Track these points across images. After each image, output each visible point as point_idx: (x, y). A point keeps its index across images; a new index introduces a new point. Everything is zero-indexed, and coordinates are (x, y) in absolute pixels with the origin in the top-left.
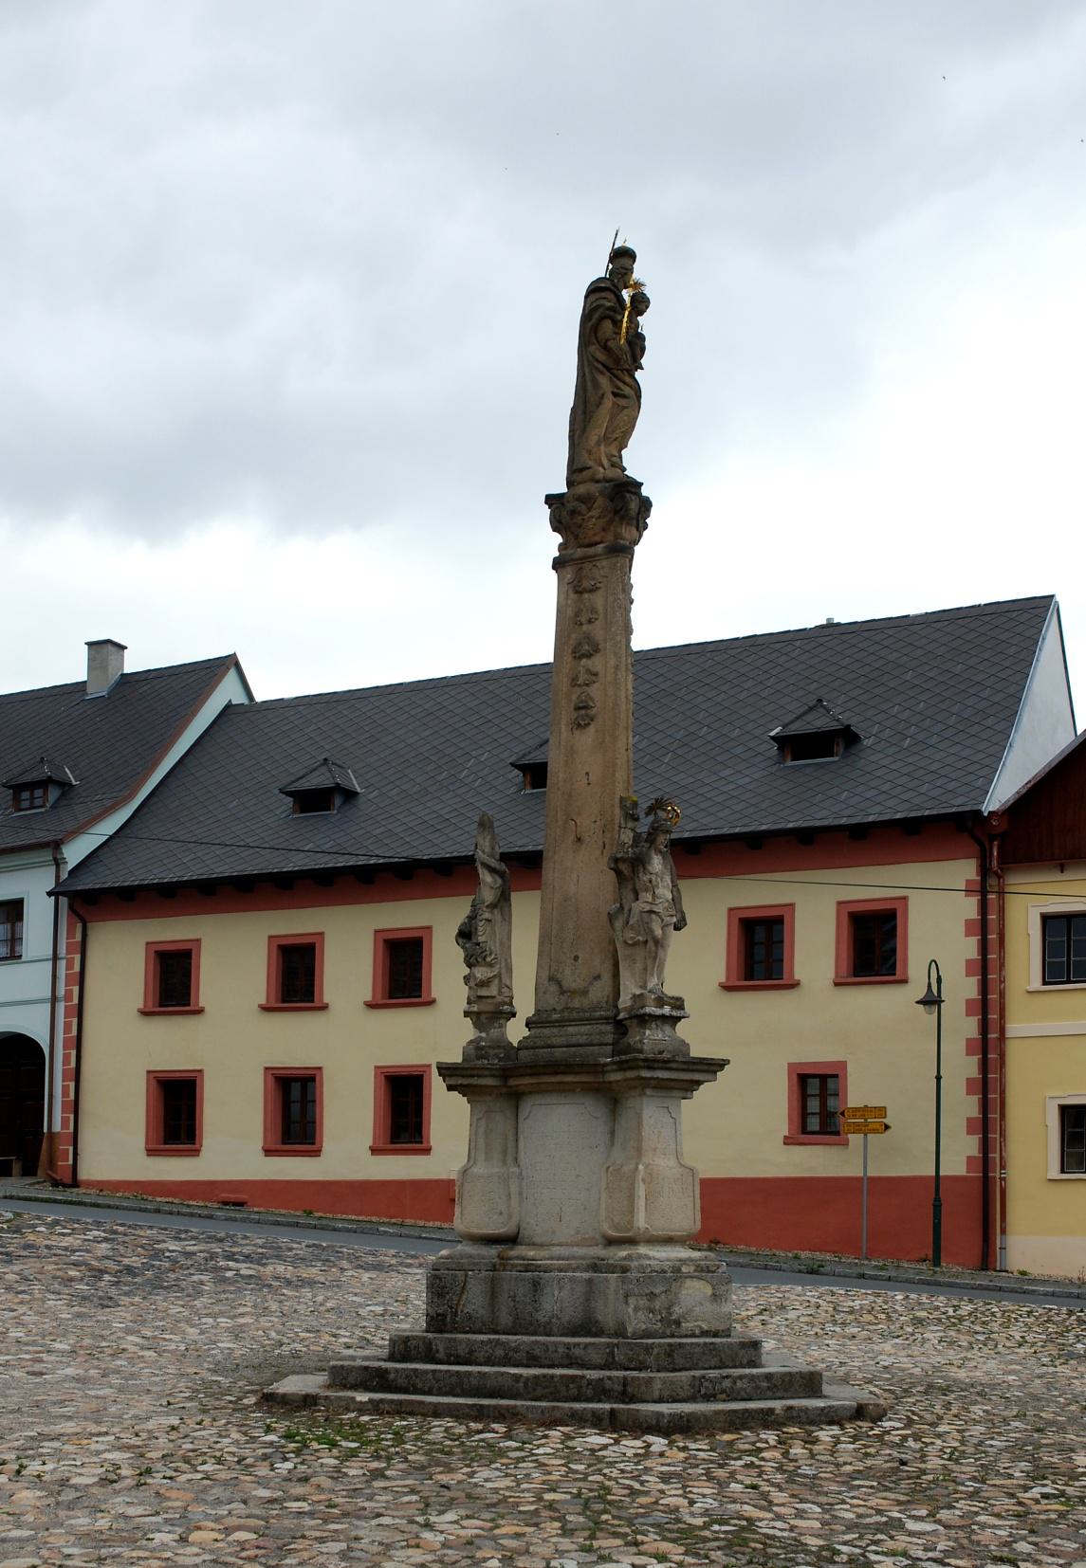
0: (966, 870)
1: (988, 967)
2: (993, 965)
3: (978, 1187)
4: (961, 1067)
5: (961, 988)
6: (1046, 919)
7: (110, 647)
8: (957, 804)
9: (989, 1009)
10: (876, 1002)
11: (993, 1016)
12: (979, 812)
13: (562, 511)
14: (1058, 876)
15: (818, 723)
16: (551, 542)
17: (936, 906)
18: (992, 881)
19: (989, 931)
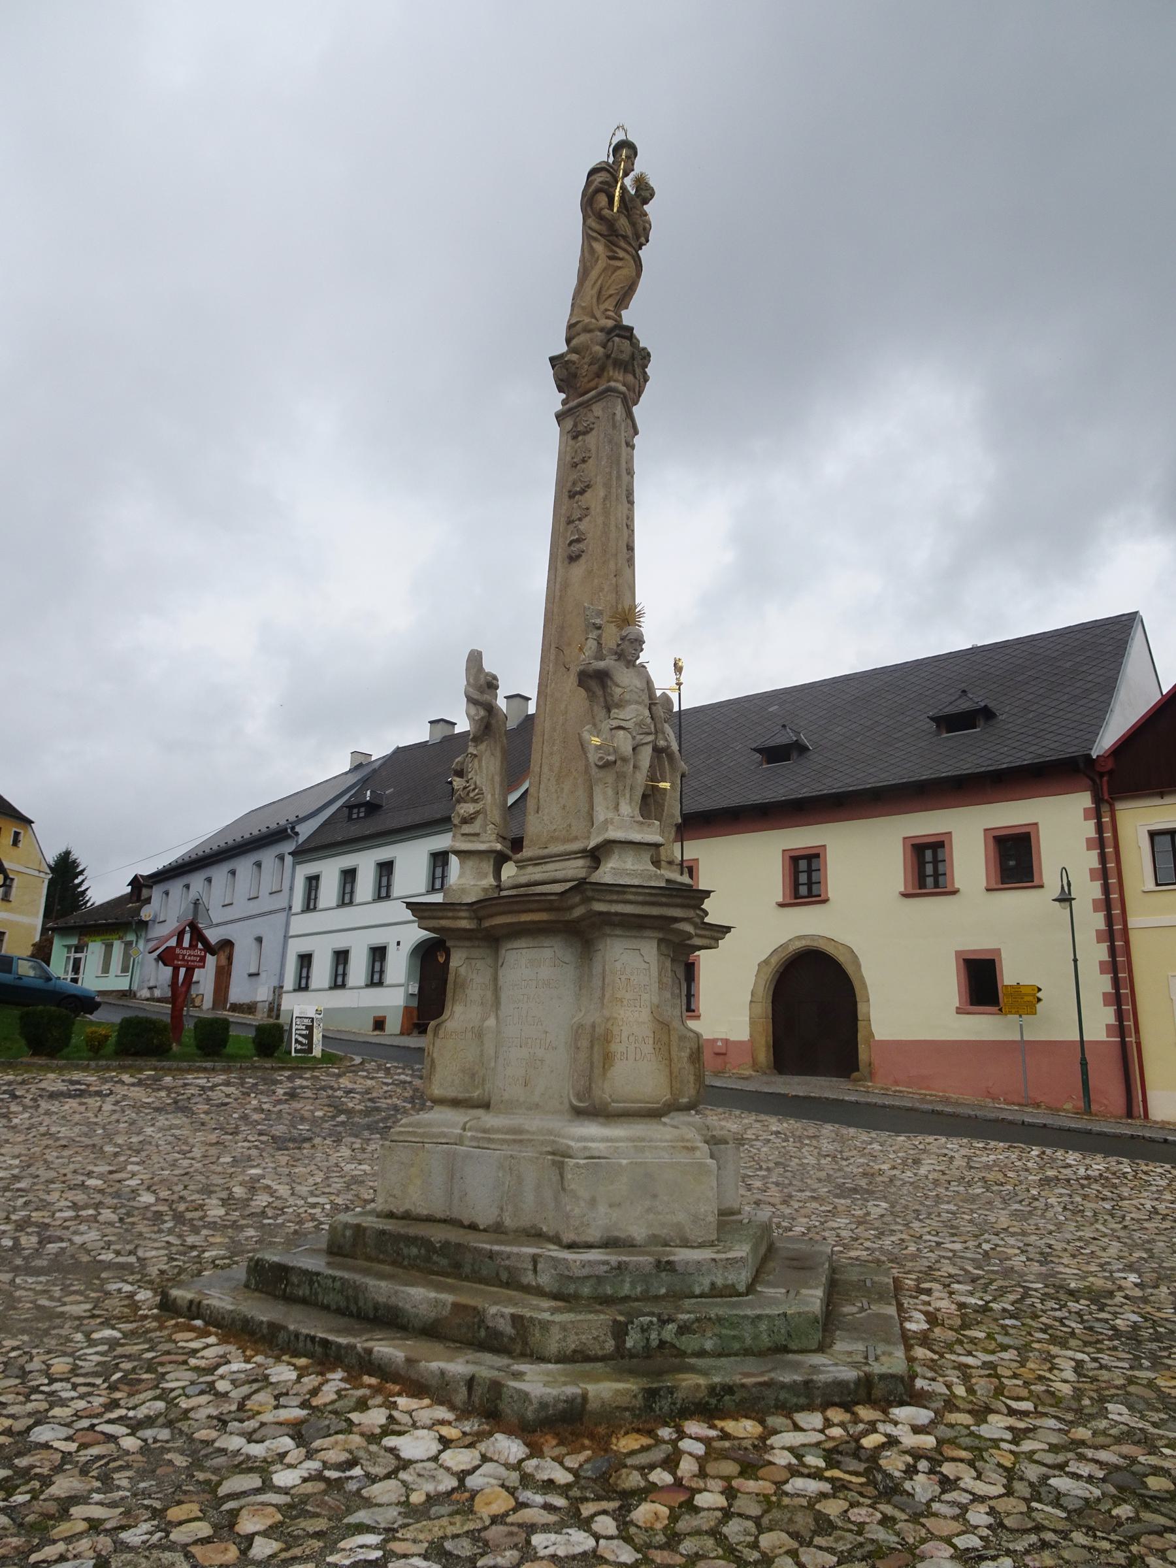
0: (1084, 800)
1: (1109, 872)
2: (1113, 873)
3: (1116, 1053)
5: (1088, 891)
6: (1153, 835)
7: (518, 699)
8: (1072, 751)
9: (1113, 906)
10: (1016, 900)
11: (1116, 912)
12: (1089, 755)
13: (566, 373)
14: (1157, 801)
15: (965, 705)
16: (556, 400)
17: (1061, 825)
18: (1105, 808)
19: (1106, 845)
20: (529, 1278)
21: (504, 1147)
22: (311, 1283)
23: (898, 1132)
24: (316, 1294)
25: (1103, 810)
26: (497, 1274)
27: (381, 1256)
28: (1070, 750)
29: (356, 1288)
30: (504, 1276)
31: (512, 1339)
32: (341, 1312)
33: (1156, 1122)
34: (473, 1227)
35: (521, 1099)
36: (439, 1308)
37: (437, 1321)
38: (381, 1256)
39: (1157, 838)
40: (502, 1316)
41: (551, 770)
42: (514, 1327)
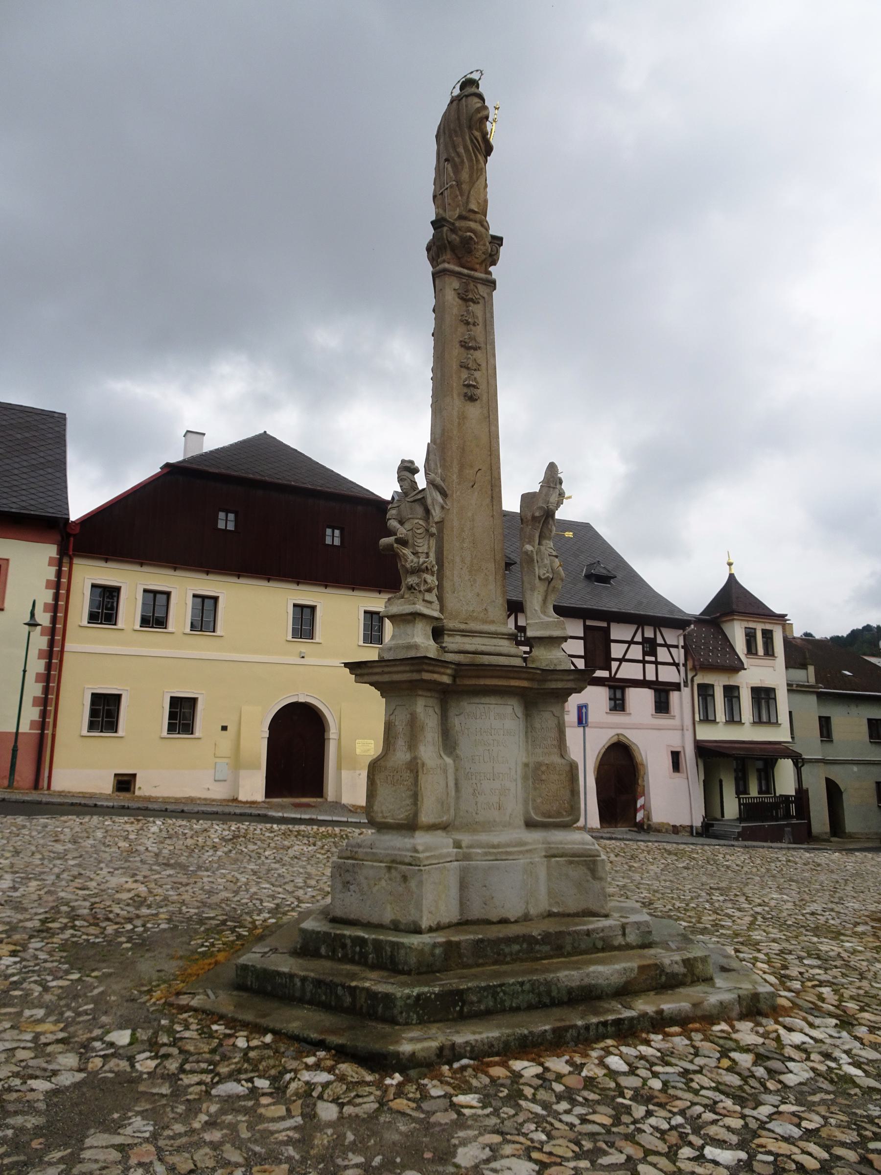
0: (51, 551)
1: (59, 607)
4: (37, 666)
11: (58, 638)
14: (137, 568)
18: (66, 560)
19: (60, 588)
20: (619, 941)
21: (520, 857)
22: (495, 995)
23: (6, 815)
24: (502, 1001)
25: (64, 561)
26: (594, 944)
27: (481, 961)
28: (51, 510)
29: (547, 983)
30: (600, 945)
31: (685, 975)
32: (531, 1007)
33: (55, 792)
34: (504, 921)
35: (497, 819)
36: (628, 974)
37: (627, 983)
38: (481, 961)
39: (212, 601)
40: (676, 963)
41: (463, 561)
42: (685, 967)
